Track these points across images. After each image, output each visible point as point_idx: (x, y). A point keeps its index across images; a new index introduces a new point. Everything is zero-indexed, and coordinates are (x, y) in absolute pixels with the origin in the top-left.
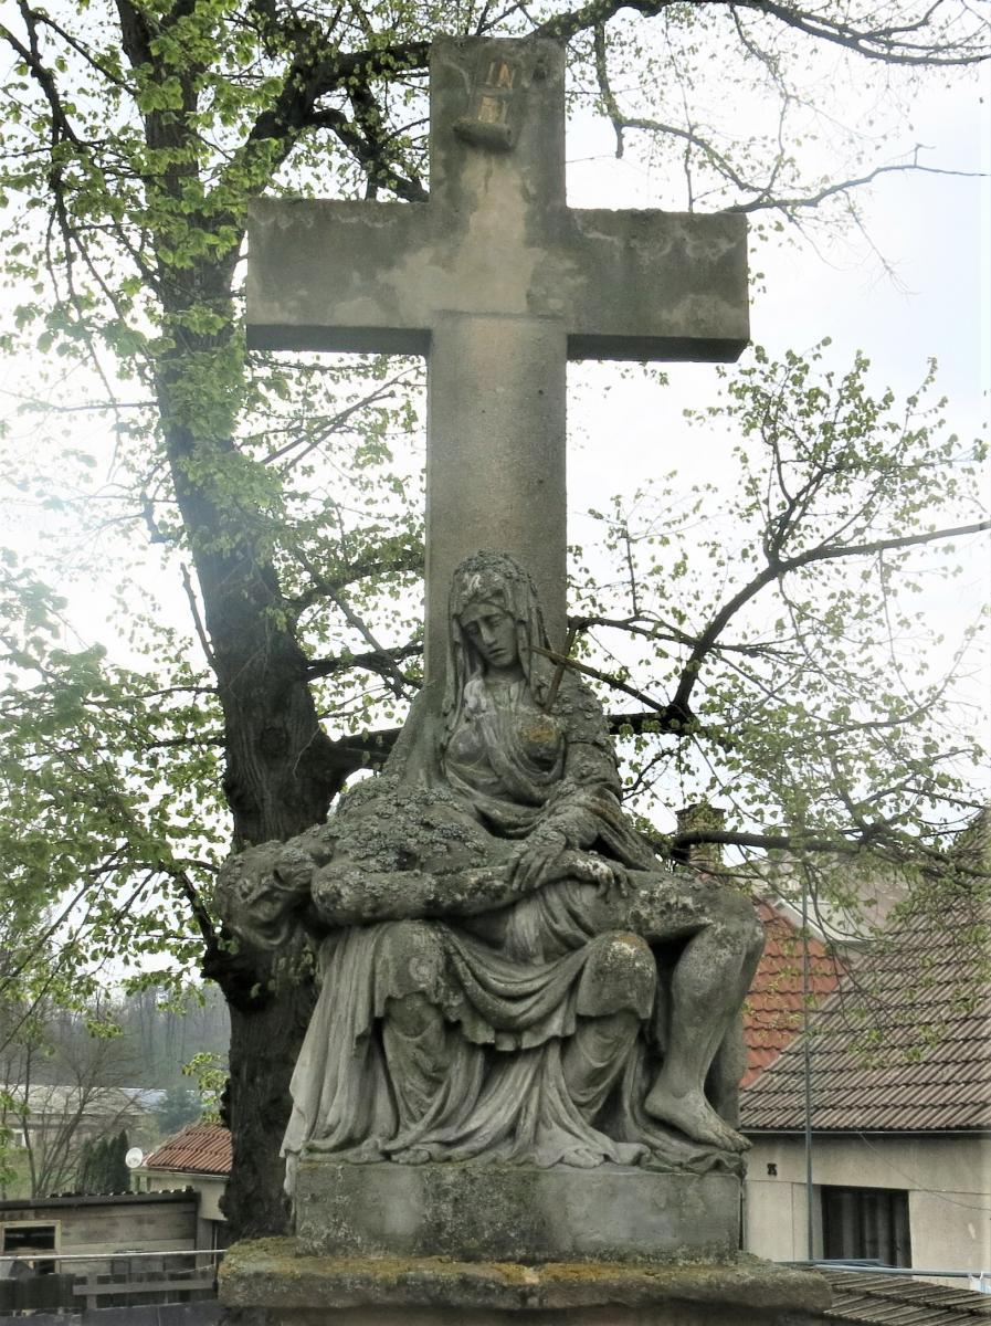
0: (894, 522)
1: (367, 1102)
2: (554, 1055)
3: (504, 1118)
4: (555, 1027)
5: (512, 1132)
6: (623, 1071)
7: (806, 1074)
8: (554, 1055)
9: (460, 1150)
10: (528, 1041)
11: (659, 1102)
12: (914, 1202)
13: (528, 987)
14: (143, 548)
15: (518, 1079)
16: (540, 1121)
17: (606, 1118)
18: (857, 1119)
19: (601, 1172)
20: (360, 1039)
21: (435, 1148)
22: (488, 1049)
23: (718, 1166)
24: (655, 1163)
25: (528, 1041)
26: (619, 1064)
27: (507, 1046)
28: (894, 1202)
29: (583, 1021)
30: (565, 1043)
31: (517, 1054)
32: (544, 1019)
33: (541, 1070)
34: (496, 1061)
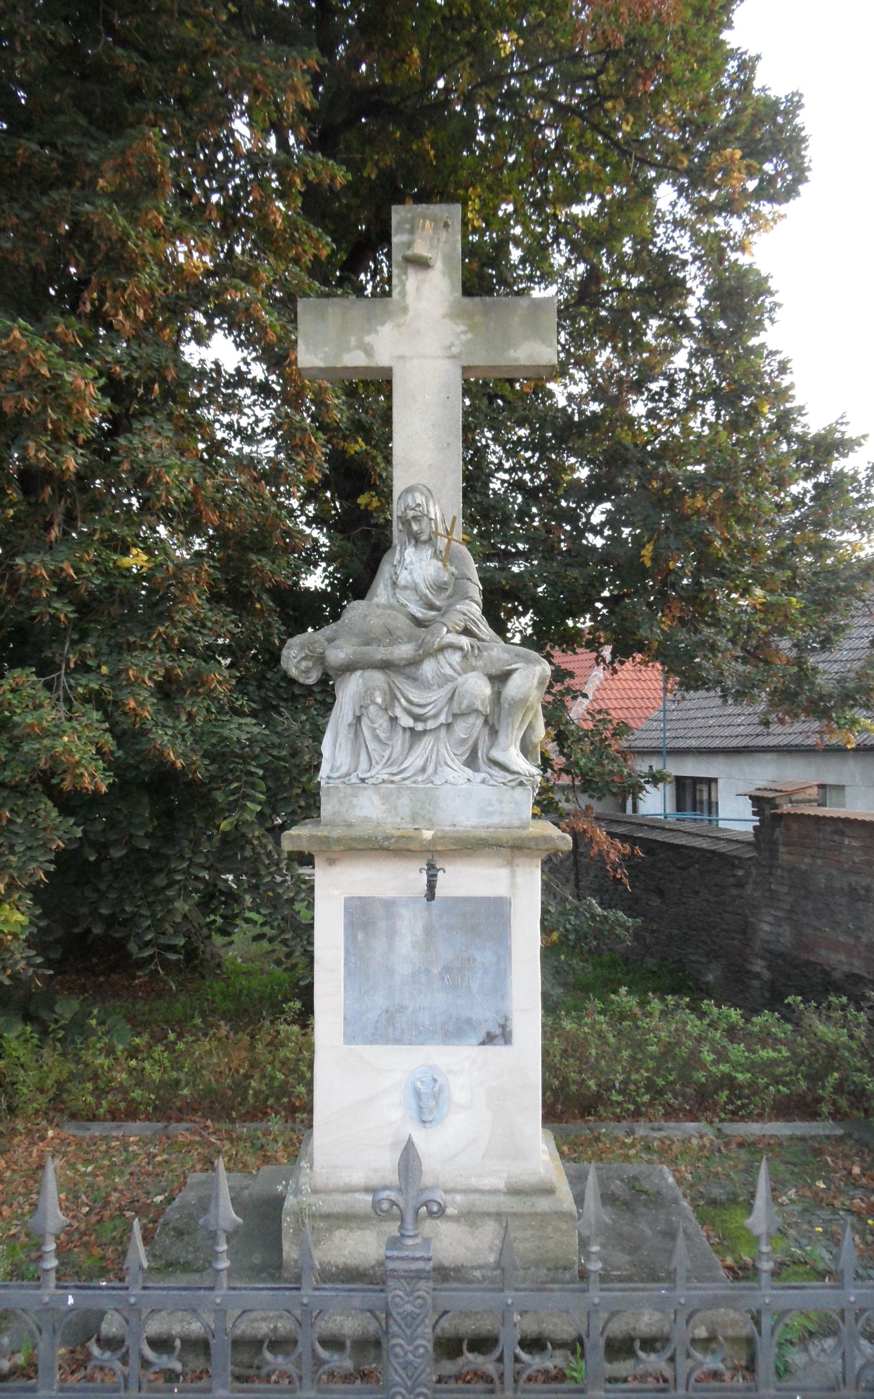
0: (779, 357)
1: (356, 756)
2: (443, 732)
3: (420, 763)
4: (442, 719)
5: (423, 769)
6: (477, 740)
7: (665, 720)
8: (443, 732)
9: (396, 778)
10: (431, 725)
11: (496, 754)
12: (721, 783)
13: (429, 700)
14: (402, 358)
15: (427, 742)
16: (437, 764)
17: (471, 762)
18: (694, 743)
19: (466, 786)
20: (350, 725)
21: (386, 777)
22: (412, 729)
23: (521, 784)
24: (492, 782)
25: (431, 725)
26: (475, 735)
27: (420, 727)
28: (711, 782)
29: (455, 716)
30: (449, 726)
31: (425, 732)
32: (436, 716)
33: (437, 739)
34: (415, 735)
